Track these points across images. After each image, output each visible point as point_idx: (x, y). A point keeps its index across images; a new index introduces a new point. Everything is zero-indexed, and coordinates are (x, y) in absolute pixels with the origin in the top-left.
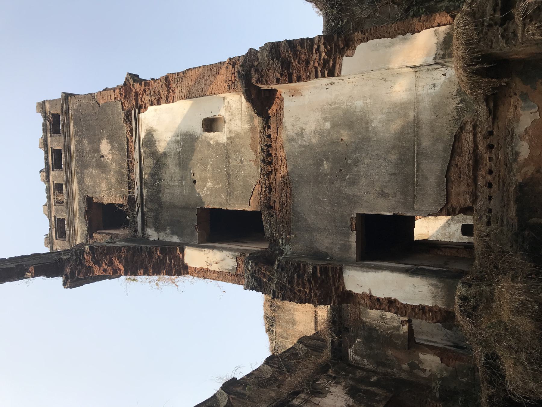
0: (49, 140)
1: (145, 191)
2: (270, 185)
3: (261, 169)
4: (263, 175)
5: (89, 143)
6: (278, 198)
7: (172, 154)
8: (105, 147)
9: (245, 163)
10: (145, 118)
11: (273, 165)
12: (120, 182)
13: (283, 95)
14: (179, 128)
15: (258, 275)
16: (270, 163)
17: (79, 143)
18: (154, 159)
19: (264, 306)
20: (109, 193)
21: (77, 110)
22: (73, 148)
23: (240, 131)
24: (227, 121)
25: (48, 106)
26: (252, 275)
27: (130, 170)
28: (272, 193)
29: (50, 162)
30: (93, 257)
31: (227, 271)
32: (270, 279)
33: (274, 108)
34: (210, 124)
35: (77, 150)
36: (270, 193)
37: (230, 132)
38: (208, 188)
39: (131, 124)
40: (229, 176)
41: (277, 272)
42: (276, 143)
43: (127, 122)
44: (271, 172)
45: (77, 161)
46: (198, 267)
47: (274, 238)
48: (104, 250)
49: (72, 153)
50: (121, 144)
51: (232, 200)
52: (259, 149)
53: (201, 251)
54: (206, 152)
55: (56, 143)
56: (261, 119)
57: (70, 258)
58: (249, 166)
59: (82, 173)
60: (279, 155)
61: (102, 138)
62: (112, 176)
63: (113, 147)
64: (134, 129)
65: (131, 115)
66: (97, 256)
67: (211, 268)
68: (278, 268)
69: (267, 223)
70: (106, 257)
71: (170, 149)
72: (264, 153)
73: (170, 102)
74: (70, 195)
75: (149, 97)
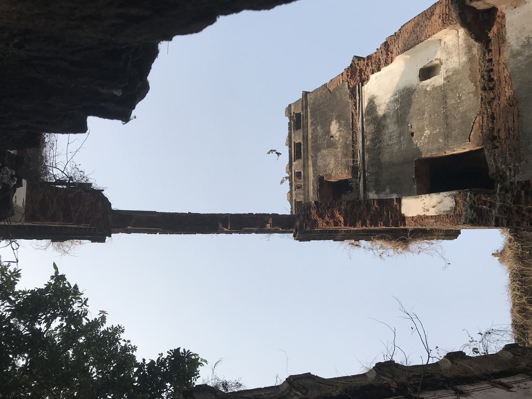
0: (293, 135)
1: (366, 157)
2: (493, 113)
3: (482, 99)
4: (485, 103)
5: (322, 128)
6: (503, 125)
7: (391, 114)
8: (334, 128)
9: (463, 98)
10: (367, 88)
11: (496, 90)
12: (345, 155)
13: (504, 11)
14: (397, 86)
15: (478, 205)
16: (492, 89)
17: (314, 130)
18: (375, 124)
19: (512, 312)
20: (338, 173)
21: (313, 103)
22: (310, 136)
23: (457, 67)
24: (443, 62)
25: (293, 107)
26: (471, 207)
27: (354, 141)
28: (495, 121)
29: (293, 154)
30: (318, 211)
31: (445, 214)
32: (492, 205)
33: (495, 29)
34: (427, 73)
35: (312, 137)
36: (493, 122)
37: (446, 72)
38: (425, 137)
39: (355, 98)
40: (446, 117)
41: (500, 195)
42: (499, 64)
43: (352, 98)
44: (493, 99)
45: (312, 147)
46: (415, 215)
47: (501, 173)
48: (327, 204)
49: (309, 141)
50: (347, 120)
51: (450, 141)
52: (479, 77)
53: (418, 198)
54: (423, 100)
55: (298, 139)
56: (480, 45)
57: (300, 214)
58: (468, 100)
59: (316, 156)
60: (502, 77)
61: (332, 120)
62: (339, 150)
63: (340, 126)
64: (358, 102)
65: (355, 91)
66: (321, 210)
67: (428, 214)
68: (500, 191)
69: (490, 156)
70: (328, 210)
71: (389, 109)
72: (484, 79)
73: (389, 64)
74: (306, 178)
75: (370, 67)
